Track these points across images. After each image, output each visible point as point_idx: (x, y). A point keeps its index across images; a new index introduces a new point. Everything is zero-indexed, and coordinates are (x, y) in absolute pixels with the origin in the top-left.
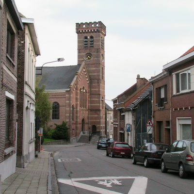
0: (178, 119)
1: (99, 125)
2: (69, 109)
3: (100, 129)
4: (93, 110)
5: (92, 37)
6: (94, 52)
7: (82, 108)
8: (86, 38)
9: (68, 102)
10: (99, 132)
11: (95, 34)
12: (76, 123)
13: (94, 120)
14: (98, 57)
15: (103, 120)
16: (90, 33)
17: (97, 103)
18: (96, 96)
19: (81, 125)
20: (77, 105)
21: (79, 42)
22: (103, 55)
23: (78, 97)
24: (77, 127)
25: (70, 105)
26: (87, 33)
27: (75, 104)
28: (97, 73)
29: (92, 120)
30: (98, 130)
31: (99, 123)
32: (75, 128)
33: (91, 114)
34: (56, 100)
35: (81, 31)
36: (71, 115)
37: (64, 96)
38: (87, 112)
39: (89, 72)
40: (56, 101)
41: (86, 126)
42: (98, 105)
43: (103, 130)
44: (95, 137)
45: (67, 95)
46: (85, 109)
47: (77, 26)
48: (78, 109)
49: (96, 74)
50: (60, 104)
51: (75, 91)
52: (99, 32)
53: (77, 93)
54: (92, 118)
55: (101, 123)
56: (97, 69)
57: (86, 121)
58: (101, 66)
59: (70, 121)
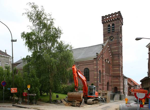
0: (149, 105)
1: (119, 87)
2: (96, 73)
3: (120, 90)
4: (115, 76)
5: (113, 25)
6: (115, 35)
7: (107, 74)
8: (109, 26)
9: (96, 67)
10: (120, 92)
11: (115, 21)
12: (103, 85)
13: (116, 84)
14: (119, 59)
15: (122, 84)
16: (112, 21)
17: (118, 71)
18: (117, 66)
19: (106, 87)
20: (103, 70)
21: (104, 30)
22: (121, 38)
23: (104, 65)
24: (103, 88)
25: (97, 70)
26: (110, 22)
27: (101, 70)
28: (117, 50)
29: (114, 84)
30: (118, 91)
31: (120, 85)
32: (102, 89)
33: (113, 79)
34: (86, 67)
35: (105, 21)
36: (98, 77)
37: (93, 63)
38: (111, 78)
39: (111, 50)
40: (86, 67)
41: (110, 88)
42: (119, 72)
43: (122, 91)
44: (117, 95)
45: (95, 62)
46: (109, 75)
47: (102, 18)
48: (104, 74)
49: (117, 50)
50: (90, 69)
51: (101, 60)
52: (119, 20)
53: (103, 61)
54: (114, 82)
55: (121, 85)
56: (117, 47)
57: (110, 84)
58: (121, 67)
59: (97, 82)
